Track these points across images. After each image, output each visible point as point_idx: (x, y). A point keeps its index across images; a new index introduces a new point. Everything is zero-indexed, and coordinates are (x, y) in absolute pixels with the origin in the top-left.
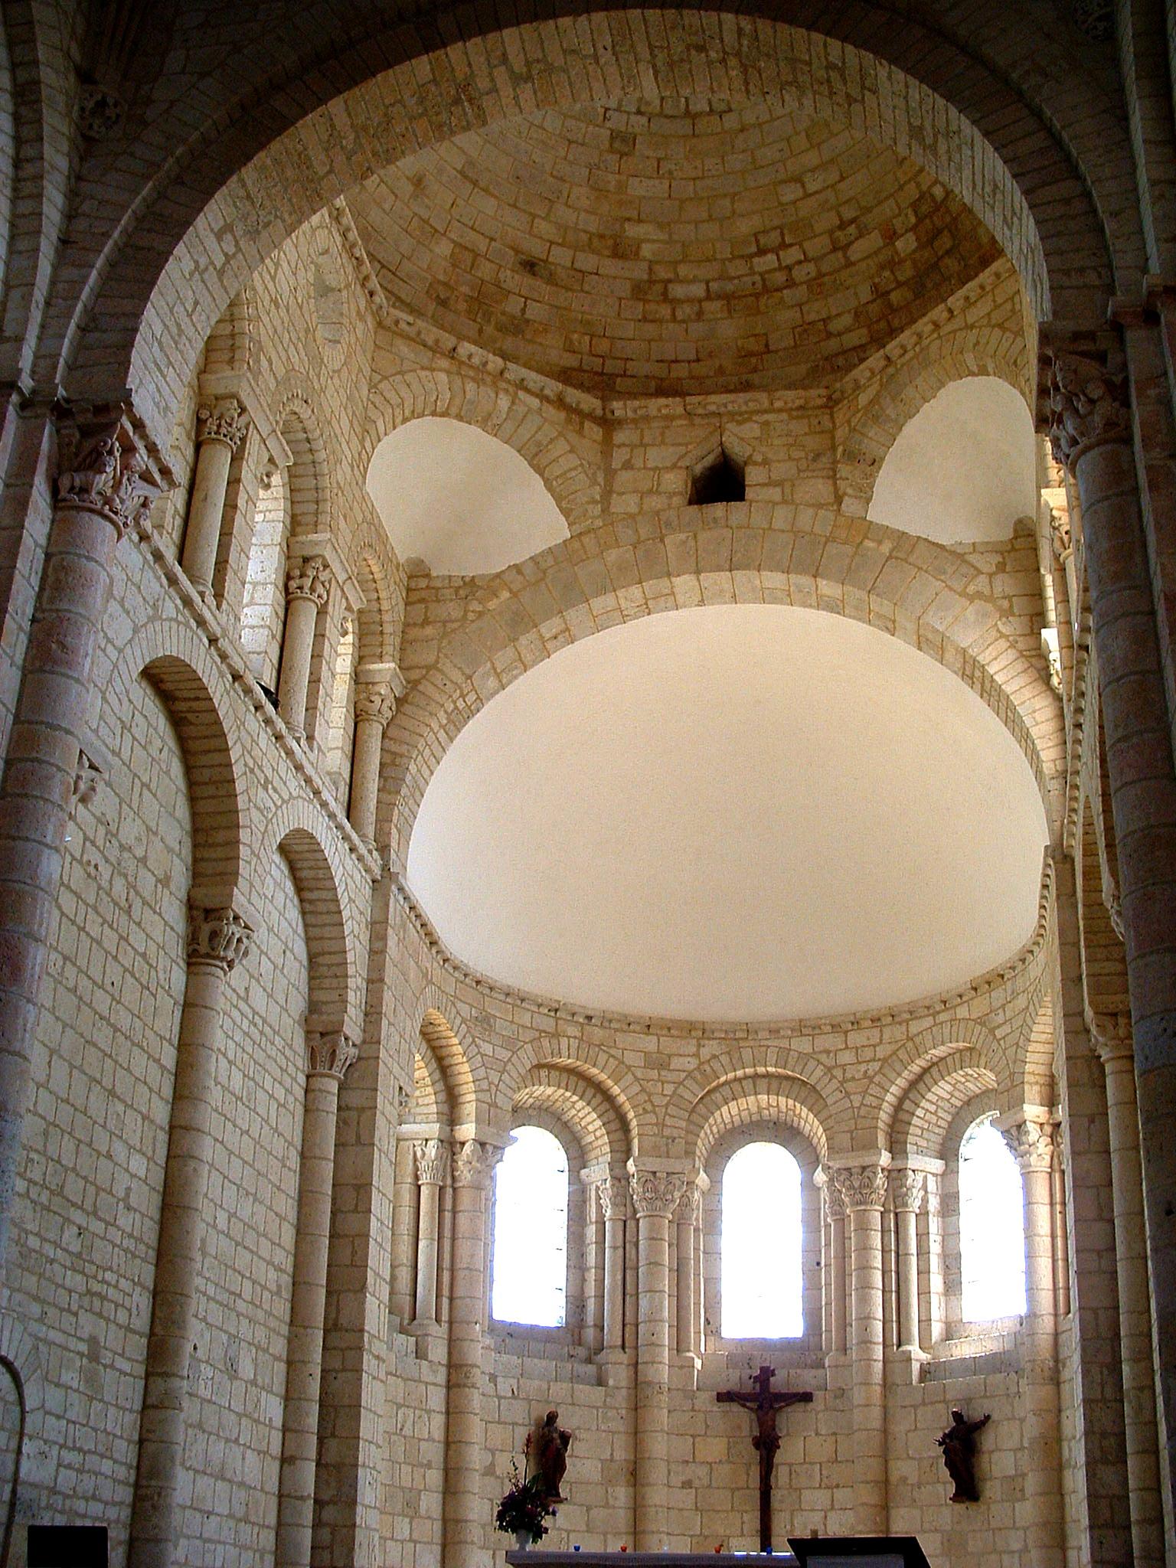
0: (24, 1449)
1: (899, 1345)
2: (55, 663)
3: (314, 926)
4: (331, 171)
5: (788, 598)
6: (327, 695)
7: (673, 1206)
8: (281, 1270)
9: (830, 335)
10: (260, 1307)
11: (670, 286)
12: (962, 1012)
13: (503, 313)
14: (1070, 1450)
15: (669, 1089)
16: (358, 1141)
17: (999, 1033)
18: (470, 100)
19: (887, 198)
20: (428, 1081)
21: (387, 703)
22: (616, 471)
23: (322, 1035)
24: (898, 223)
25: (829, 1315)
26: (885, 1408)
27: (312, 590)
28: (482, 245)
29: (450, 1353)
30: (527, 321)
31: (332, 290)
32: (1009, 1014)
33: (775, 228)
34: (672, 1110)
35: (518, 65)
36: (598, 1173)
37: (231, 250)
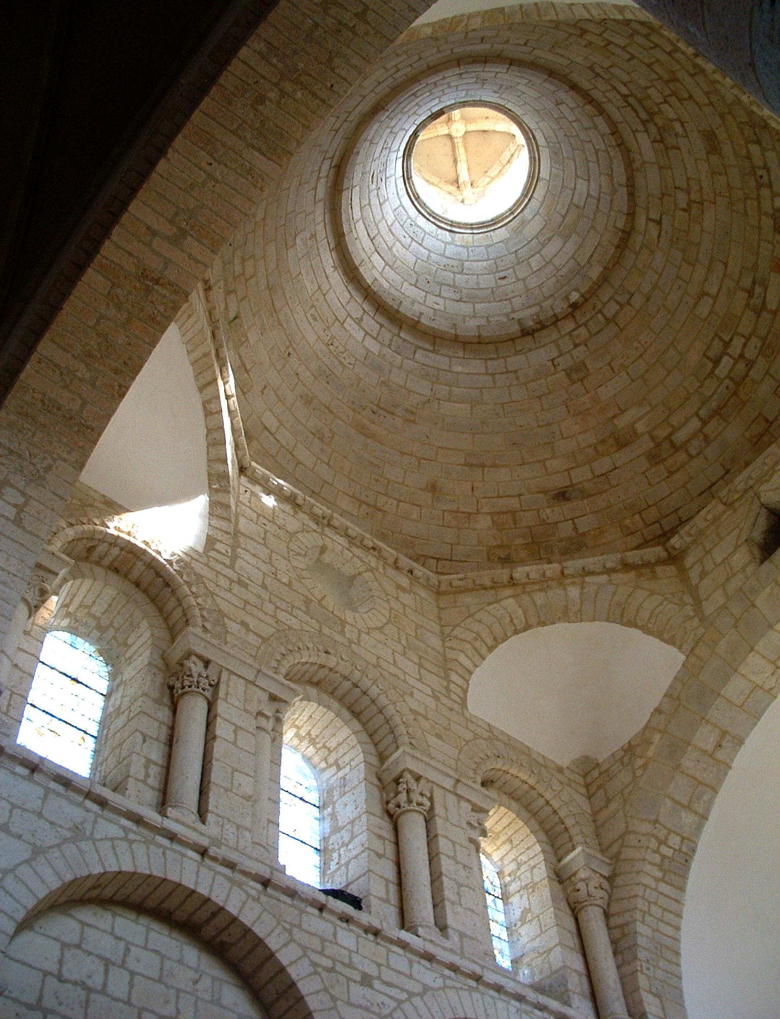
4: (84, 403)
11: (674, 437)
13: (561, 541)
18: (157, 282)
19: (759, 246)
22: (697, 586)
27: (410, 801)
28: (514, 503)
30: (583, 534)
31: (354, 577)
33: (713, 338)
37: (21, 500)
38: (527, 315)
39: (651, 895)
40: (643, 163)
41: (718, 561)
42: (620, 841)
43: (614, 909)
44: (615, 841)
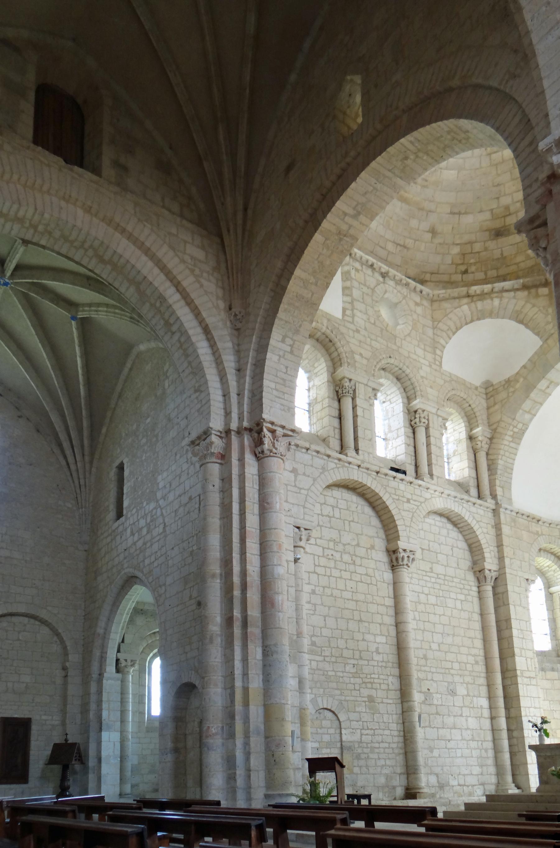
0: (342, 732)
2: (266, 510)
3: (466, 535)
8: (477, 656)
16: (504, 605)
18: (345, 236)
21: (484, 442)
23: (480, 571)
27: (420, 422)
30: (505, 257)
35: (351, 211)
37: (291, 342)
39: (506, 448)
42: (497, 424)
43: (490, 452)
44: (495, 423)
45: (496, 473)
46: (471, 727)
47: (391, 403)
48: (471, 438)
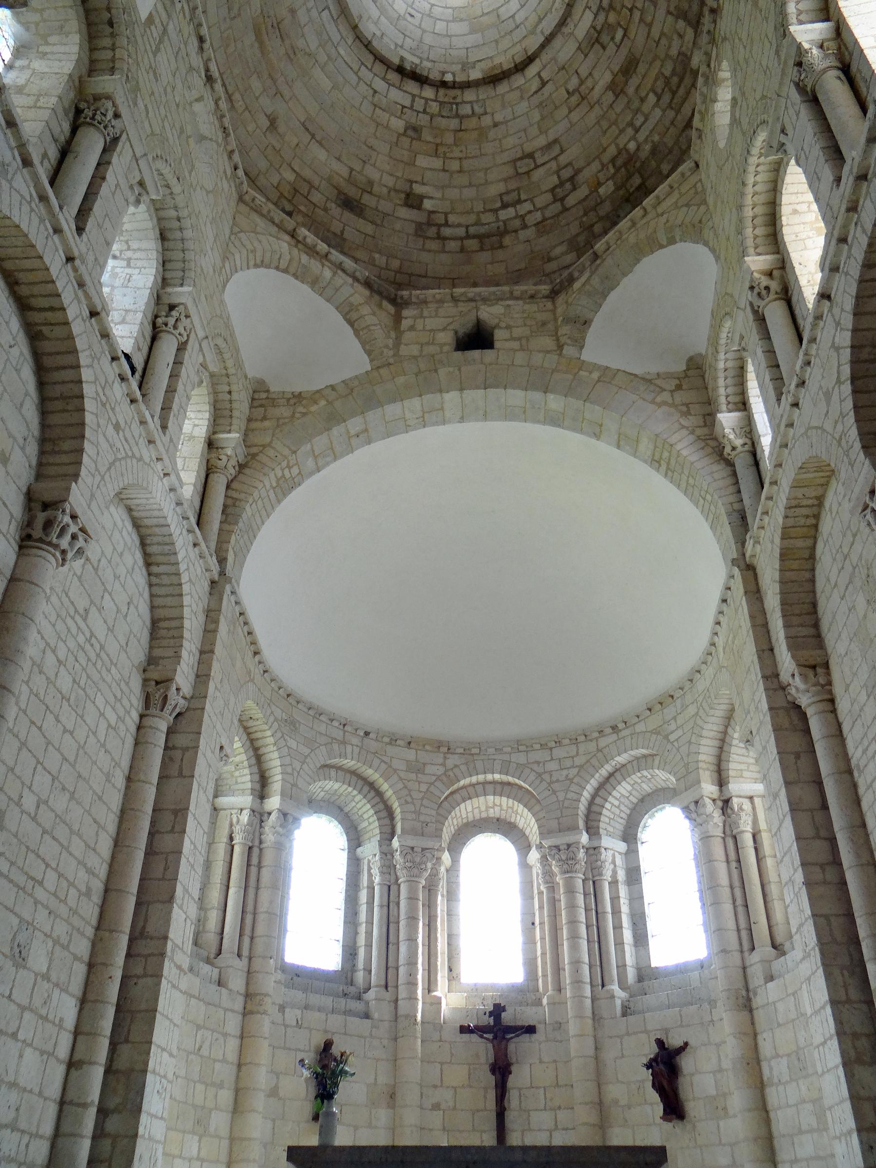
1: (603, 986)
5: (523, 415)
6: (181, 407)
7: (426, 874)
8: (93, 874)
9: (550, 260)
10: (64, 901)
12: (640, 727)
14: (771, 1069)
15: (424, 787)
16: (181, 775)
17: (672, 737)
20: (246, 764)
24: (602, 177)
25: (544, 963)
26: (595, 1037)
27: (175, 327)
29: (247, 984)
32: (679, 722)
34: (425, 802)
36: (370, 850)
38: (411, 60)
39: (263, 493)
40: (572, 34)
41: (428, 328)
45: (236, 523)
46: (22, 1082)
47: (129, 266)
48: (211, 444)
